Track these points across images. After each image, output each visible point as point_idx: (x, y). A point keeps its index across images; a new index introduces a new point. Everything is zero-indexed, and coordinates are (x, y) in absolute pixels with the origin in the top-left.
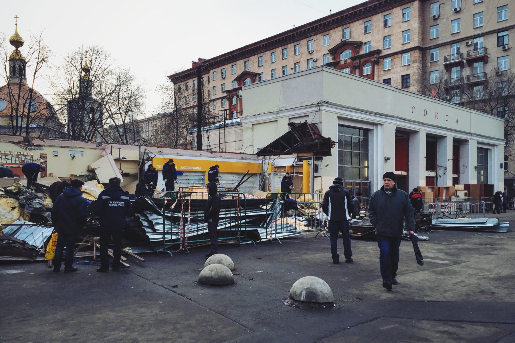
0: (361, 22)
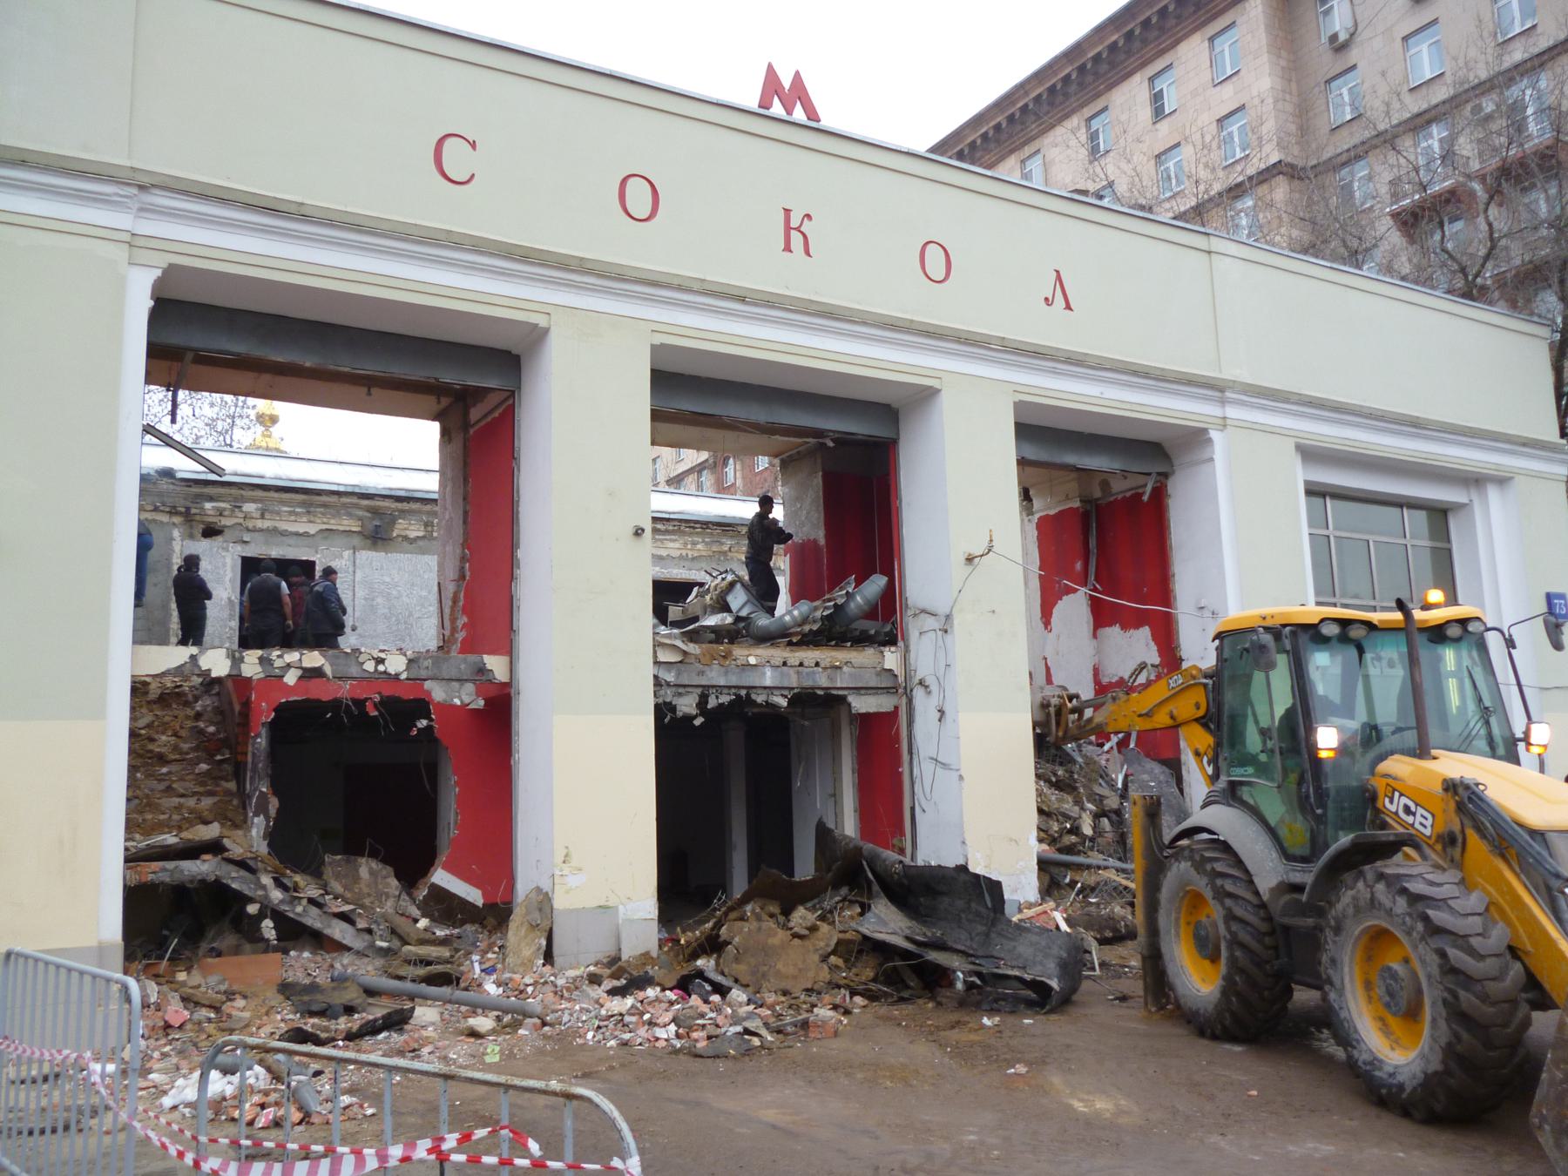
0: (1075, 121)
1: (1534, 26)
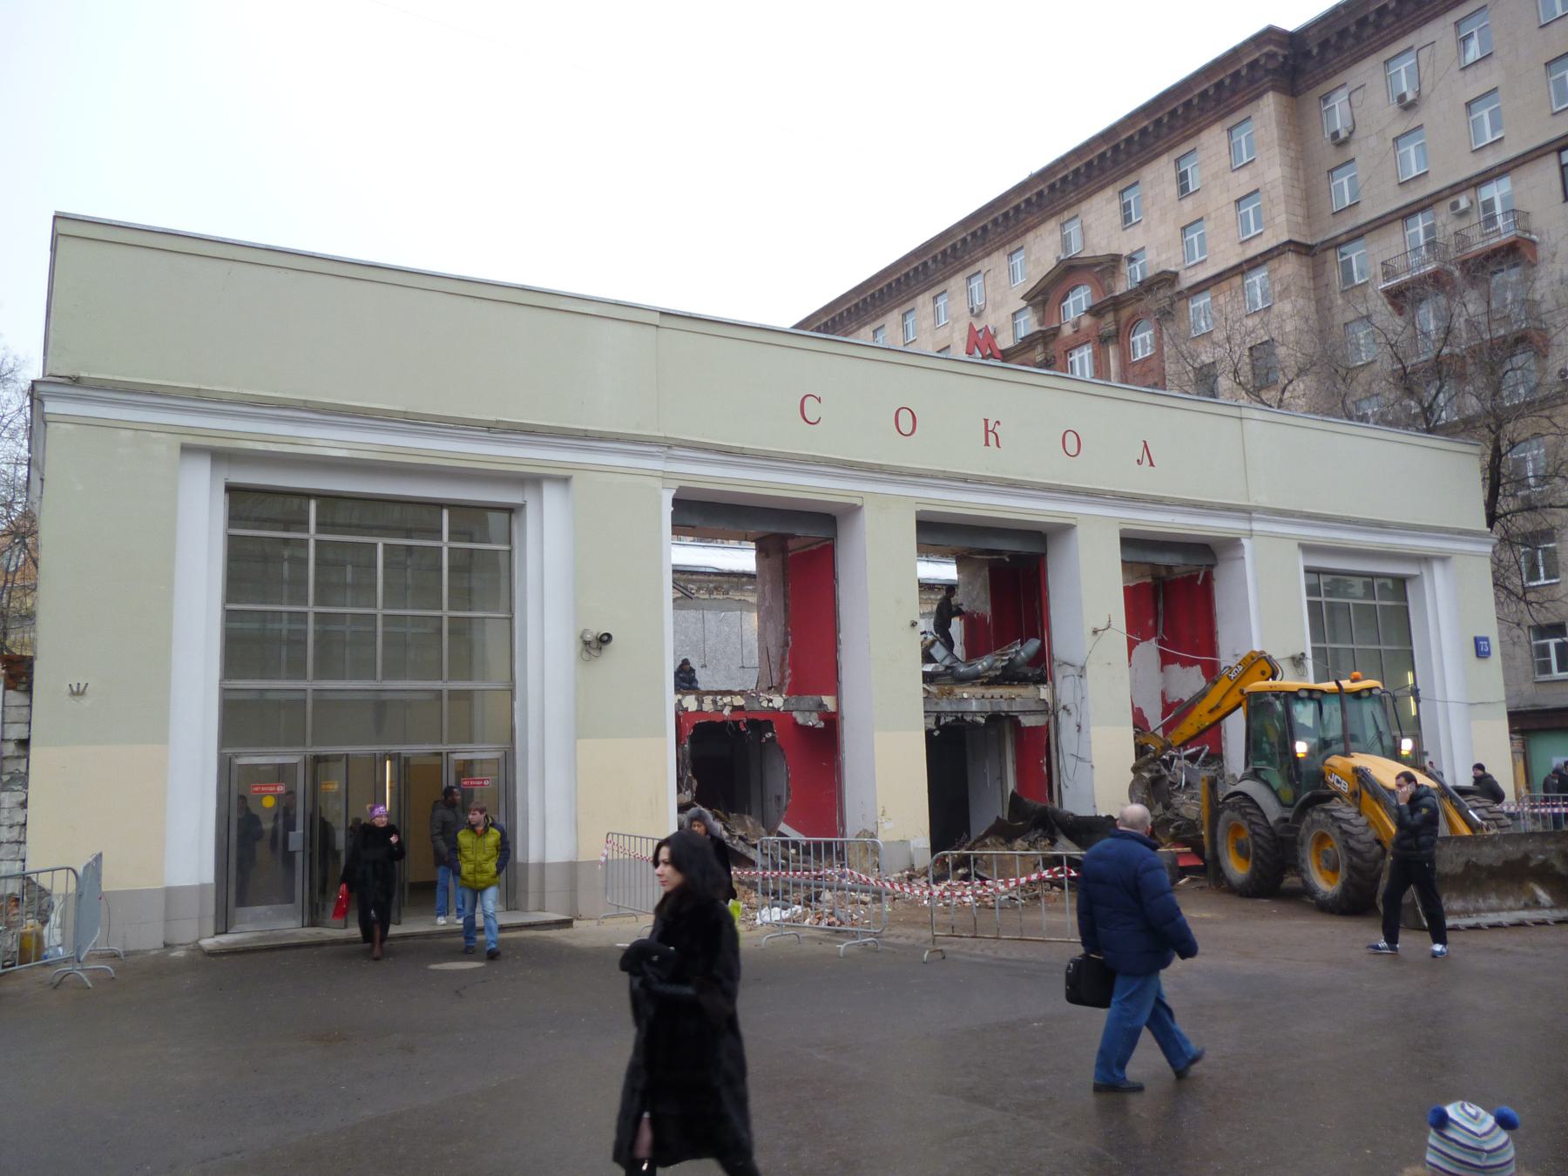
0: (1110, 192)
1: (1501, 139)
